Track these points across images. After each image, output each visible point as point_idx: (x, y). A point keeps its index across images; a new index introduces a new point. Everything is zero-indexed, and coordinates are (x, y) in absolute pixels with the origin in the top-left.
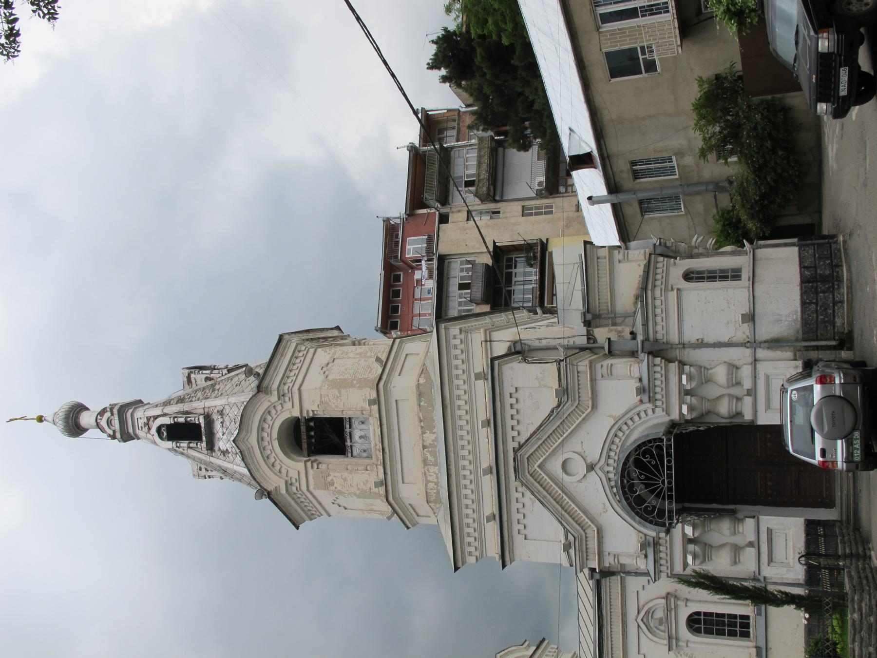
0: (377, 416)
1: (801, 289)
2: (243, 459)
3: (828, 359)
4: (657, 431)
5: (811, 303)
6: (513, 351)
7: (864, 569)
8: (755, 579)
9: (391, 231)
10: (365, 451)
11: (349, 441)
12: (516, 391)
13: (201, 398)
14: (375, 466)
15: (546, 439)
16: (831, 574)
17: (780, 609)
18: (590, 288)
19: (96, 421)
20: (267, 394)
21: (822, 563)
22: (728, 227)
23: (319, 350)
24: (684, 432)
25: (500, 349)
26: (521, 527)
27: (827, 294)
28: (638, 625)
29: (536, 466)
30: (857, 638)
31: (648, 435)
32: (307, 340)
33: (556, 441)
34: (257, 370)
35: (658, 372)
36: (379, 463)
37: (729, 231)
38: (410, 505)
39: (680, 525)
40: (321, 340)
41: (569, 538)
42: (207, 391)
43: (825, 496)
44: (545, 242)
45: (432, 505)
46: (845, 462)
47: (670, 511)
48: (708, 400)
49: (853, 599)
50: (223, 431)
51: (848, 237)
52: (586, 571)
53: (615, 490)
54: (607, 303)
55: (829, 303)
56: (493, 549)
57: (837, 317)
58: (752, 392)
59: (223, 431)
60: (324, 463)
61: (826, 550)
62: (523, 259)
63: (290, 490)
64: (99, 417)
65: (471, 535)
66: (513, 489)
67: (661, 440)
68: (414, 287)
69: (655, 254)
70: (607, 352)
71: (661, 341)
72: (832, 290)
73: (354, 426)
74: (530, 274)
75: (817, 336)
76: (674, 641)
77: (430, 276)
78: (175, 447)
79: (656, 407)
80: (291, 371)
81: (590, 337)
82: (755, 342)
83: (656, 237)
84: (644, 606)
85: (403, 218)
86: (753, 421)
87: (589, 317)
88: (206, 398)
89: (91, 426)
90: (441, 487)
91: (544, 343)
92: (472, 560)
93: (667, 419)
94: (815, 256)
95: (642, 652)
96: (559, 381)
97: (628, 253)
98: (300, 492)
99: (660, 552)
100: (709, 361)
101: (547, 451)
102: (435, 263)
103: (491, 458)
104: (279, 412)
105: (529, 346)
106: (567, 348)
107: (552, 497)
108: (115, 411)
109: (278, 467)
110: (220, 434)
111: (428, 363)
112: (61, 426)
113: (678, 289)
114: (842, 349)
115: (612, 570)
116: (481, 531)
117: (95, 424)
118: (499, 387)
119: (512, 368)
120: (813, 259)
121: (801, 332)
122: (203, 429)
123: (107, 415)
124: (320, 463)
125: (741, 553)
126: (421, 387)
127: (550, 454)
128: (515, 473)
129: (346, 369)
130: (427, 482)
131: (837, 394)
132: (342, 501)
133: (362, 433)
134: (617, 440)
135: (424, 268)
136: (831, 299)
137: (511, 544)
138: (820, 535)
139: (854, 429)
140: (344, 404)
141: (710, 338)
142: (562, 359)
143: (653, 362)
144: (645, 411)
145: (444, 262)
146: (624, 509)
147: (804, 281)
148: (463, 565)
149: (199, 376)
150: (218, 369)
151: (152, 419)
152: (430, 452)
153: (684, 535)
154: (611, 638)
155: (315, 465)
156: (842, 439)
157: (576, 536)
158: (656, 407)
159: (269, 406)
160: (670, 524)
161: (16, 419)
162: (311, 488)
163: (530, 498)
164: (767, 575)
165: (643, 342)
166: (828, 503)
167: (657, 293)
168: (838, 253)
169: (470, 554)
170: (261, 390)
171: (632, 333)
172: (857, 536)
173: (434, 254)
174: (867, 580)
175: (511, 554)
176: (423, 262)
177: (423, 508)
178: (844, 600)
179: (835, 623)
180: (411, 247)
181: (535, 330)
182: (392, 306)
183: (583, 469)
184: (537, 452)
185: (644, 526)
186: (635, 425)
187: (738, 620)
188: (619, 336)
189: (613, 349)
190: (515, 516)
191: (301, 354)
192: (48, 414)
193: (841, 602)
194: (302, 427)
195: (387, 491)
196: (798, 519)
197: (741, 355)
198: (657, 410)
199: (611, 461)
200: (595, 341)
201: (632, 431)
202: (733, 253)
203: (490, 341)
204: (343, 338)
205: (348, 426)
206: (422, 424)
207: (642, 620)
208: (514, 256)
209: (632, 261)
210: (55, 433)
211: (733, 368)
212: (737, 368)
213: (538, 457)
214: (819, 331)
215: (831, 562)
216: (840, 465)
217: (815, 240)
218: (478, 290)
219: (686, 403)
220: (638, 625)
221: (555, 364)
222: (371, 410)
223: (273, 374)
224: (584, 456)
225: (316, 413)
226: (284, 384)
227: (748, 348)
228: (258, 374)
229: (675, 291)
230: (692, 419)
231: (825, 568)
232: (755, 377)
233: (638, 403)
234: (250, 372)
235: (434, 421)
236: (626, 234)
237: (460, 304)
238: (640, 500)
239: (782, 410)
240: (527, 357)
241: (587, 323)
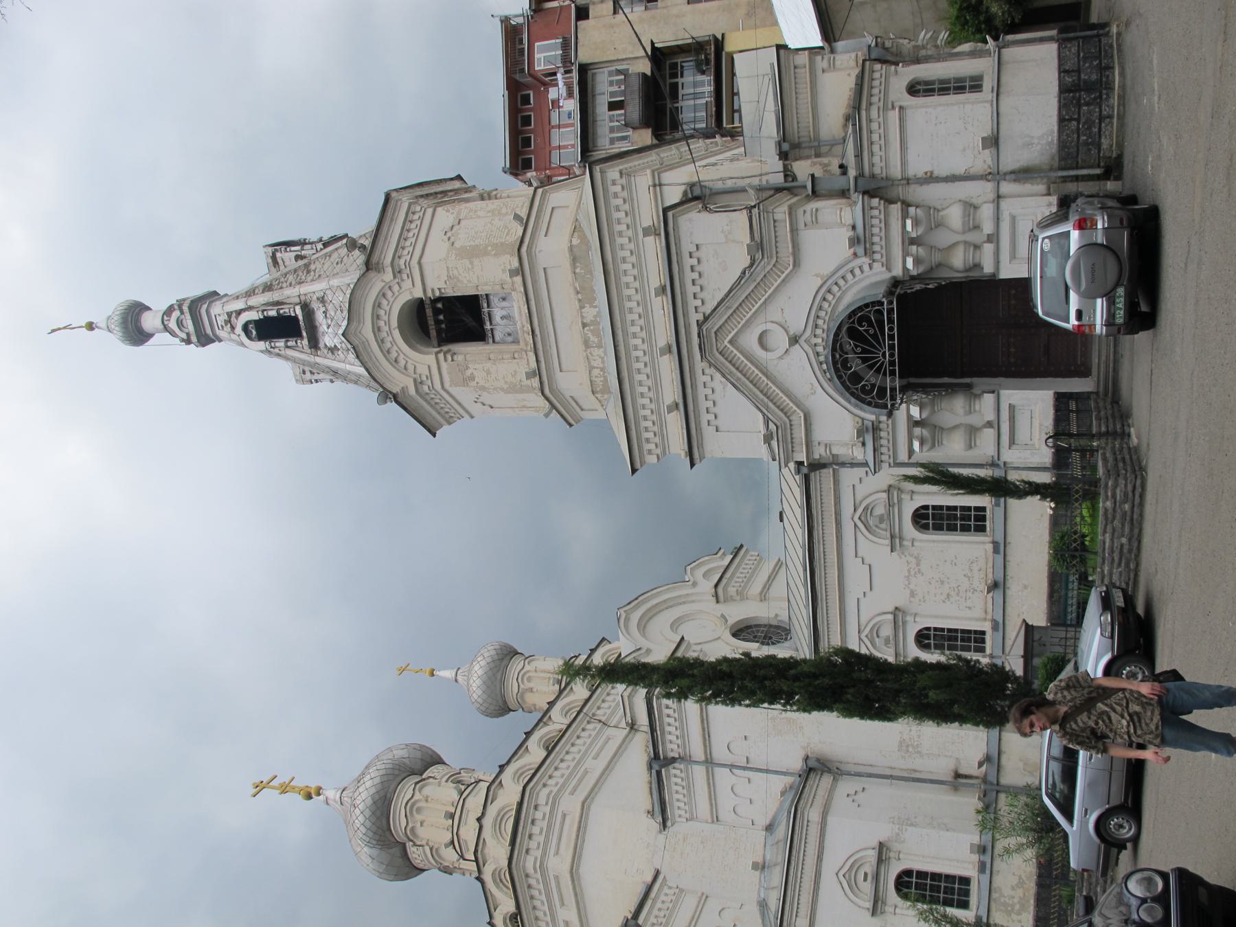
0: (522, 289)
1: (1059, 101)
2: (358, 357)
3: (1089, 193)
4: (875, 292)
5: (1071, 120)
6: (690, 196)
7: (1121, 450)
8: (993, 465)
9: (512, 34)
11: (488, 323)
12: (697, 249)
13: (294, 283)
14: (524, 353)
15: (737, 308)
16: (1083, 457)
17: (1022, 501)
18: (786, 108)
19: (163, 322)
20: (379, 272)
21: (1073, 445)
22: (965, 11)
23: (439, 210)
24: (909, 291)
25: (673, 195)
26: (711, 417)
27: (1092, 107)
28: (855, 524)
29: (726, 342)
30: (1109, 528)
31: (864, 298)
32: (422, 196)
33: (751, 310)
34: (362, 241)
35: (876, 217)
36: (529, 348)
37: (968, 17)
39: (904, 405)
40: (439, 196)
41: (770, 427)
42: (301, 274)
43: (1079, 363)
44: (720, 38)
45: (599, 396)
46: (1105, 325)
47: (893, 390)
48: (939, 249)
49: (1106, 485)
50: (327, 323)
51: (1124, 28)
52: (792, 465)
53: (824, 366)
54: (809, 127)
55: (1094, 119)
56: (678, 445)
57: (1103, 137)
58: (993, 238)
59: (327, 323)
60: (460, 354)
61: (1078, 427)
62: (691, 63)
63: (420, 391)
64: (165, 318)
65: (650, 429)
67: (881, 303)
68: (550, 110)
69: (870, 60)
70: (810, 192)
71: (879, 177)
72: (1098, 101)
73: (492, 304)
74: (702, 84)
75: (1077, 163)
76: (897, 540)
77: (570, 95)
78: (269, 348)
79: (874, 261)
80: (405, 240)
81: (788, 174)
82: (998, 173)
83: (872, 36)
84: (861, 502)
85: (528, 16)
86: (994, 275)
87: (786, 147)
88: (300, 283)
89: (157, 329)
90: (609, 373)
91: (729, 184)
92: (652, 459)
93: (887, 276)
94: (1079, 55)
95: (860, 554)
96: (751, 234)
97: (834, 58)
98: (434, 392)
99: (881, 438)
100: (940, 199)
101: (739, 323)
102: (575, 75)
103: (669, 334)
104: (397, 294)
105: (711, 189)
106: (760, 189)
107: (748, 379)
108: (185, 308)
109: (402, 363)
110: (325, 327)
111: (580, 217)
112: (117, 329)
113: (901, 108)
114: (1108, 179)
115: (823, 461)
116: (662, 424)
117: (162, 327)
118: (676, 244)
119: (690, 220)
120: (1076, 59)
121: (1057, 158)
122: (302, 323)
123: (176, 314)
124: (455, 354)
125: (978, 435)
126: (575, 250)
127: (742, 327)
128: (701, 351)
129: (476, 233)
130: (591, 368)
131: (1099, 241)
132: (486, 398)
133: (504, 313)
134: (826, 305)
135: (561, 84)
136: (1097, 114)
137: (700, 438)
138: (1072, 411)
139: (1117, 285)
140: (478, 277)
141: (941, 171)
142: (753, 204)
143: (869, 204)
144: (860, 267)
145: (587, 73)
146: (837, 390)
147: (1064, 89)
148: (641, 466)
149: (287, 254)
150: (310, 243)
151: (234, 314)
152: (591, 331)
153: (909, 417)
154: (824, 541)
155: (449, 357)
156: (1102, 298)
157: (779, 424)
158: (874, 261)
159: (383, 288)
160: (893, 405)
161: (59, 329)
162: (447, 385)
163: (721, 382)
164: (1008, 460)
165: (856, 178)
166: (1084, 372)
167: (874, 113)
168: (1110, 50)
169: (650, 452)
170: (370, 267)
171: (841, 166)
172: (1116, 410)
173: (572, 64)
174: (1124, 462)
175: (700, 448)
176: (559, 76)
177: (588, 400)
178: (1096, 487)
179: (1085, 512)
180: (542, 56)
181: (717, 167)
182: (522, 138)
184: (726, 325)
185: (861, 409)
186: (848, 285)
187: (973, 513)
188: (825, 171)
189: (817, 188)
190: (704, 405)
191: (416, 217)
192: (99, 320)
193: (1093, 489)
194: (427, 311)
195: (541, 383)
197: (981, 191)
198: (875, 265)
199: (819, 332)
200: (794, 179)
201: (844, 292)
202: (973, 54)
203: (660, 185)
204: (468, 190)
205: (485, 305)
206: (580, 296)
207: (859, 518)
208: (679, 61)
209: (839, 70)
210: (112, 343)
211: (970, 207)
212: (976, 208)
213: (728, 330)
214: (1080, 157)
215: (1083, 442)
216: (1099, 329)
217: (1080, 31)
218: (634, 109)
219: (912, 255)
220: (855, 524)
221: (745, 212)
222: (513, 283)
223: (383, 246)
224: (786, 327)
225: (443, 291)
226: (399, 257)
227: (989, 181)
228: (363, 247)
229: (897, 109)
230: (918, 275)
231: (1076, 450)
232: (998, 219)
233: (852, 257)
234: (353, 244)
235: (594, 291)
236: (829, 25)
237: (612, 130)
238: (856, 378)
239: (1030, 260)
240: (708, 204)
241: (783, 156)
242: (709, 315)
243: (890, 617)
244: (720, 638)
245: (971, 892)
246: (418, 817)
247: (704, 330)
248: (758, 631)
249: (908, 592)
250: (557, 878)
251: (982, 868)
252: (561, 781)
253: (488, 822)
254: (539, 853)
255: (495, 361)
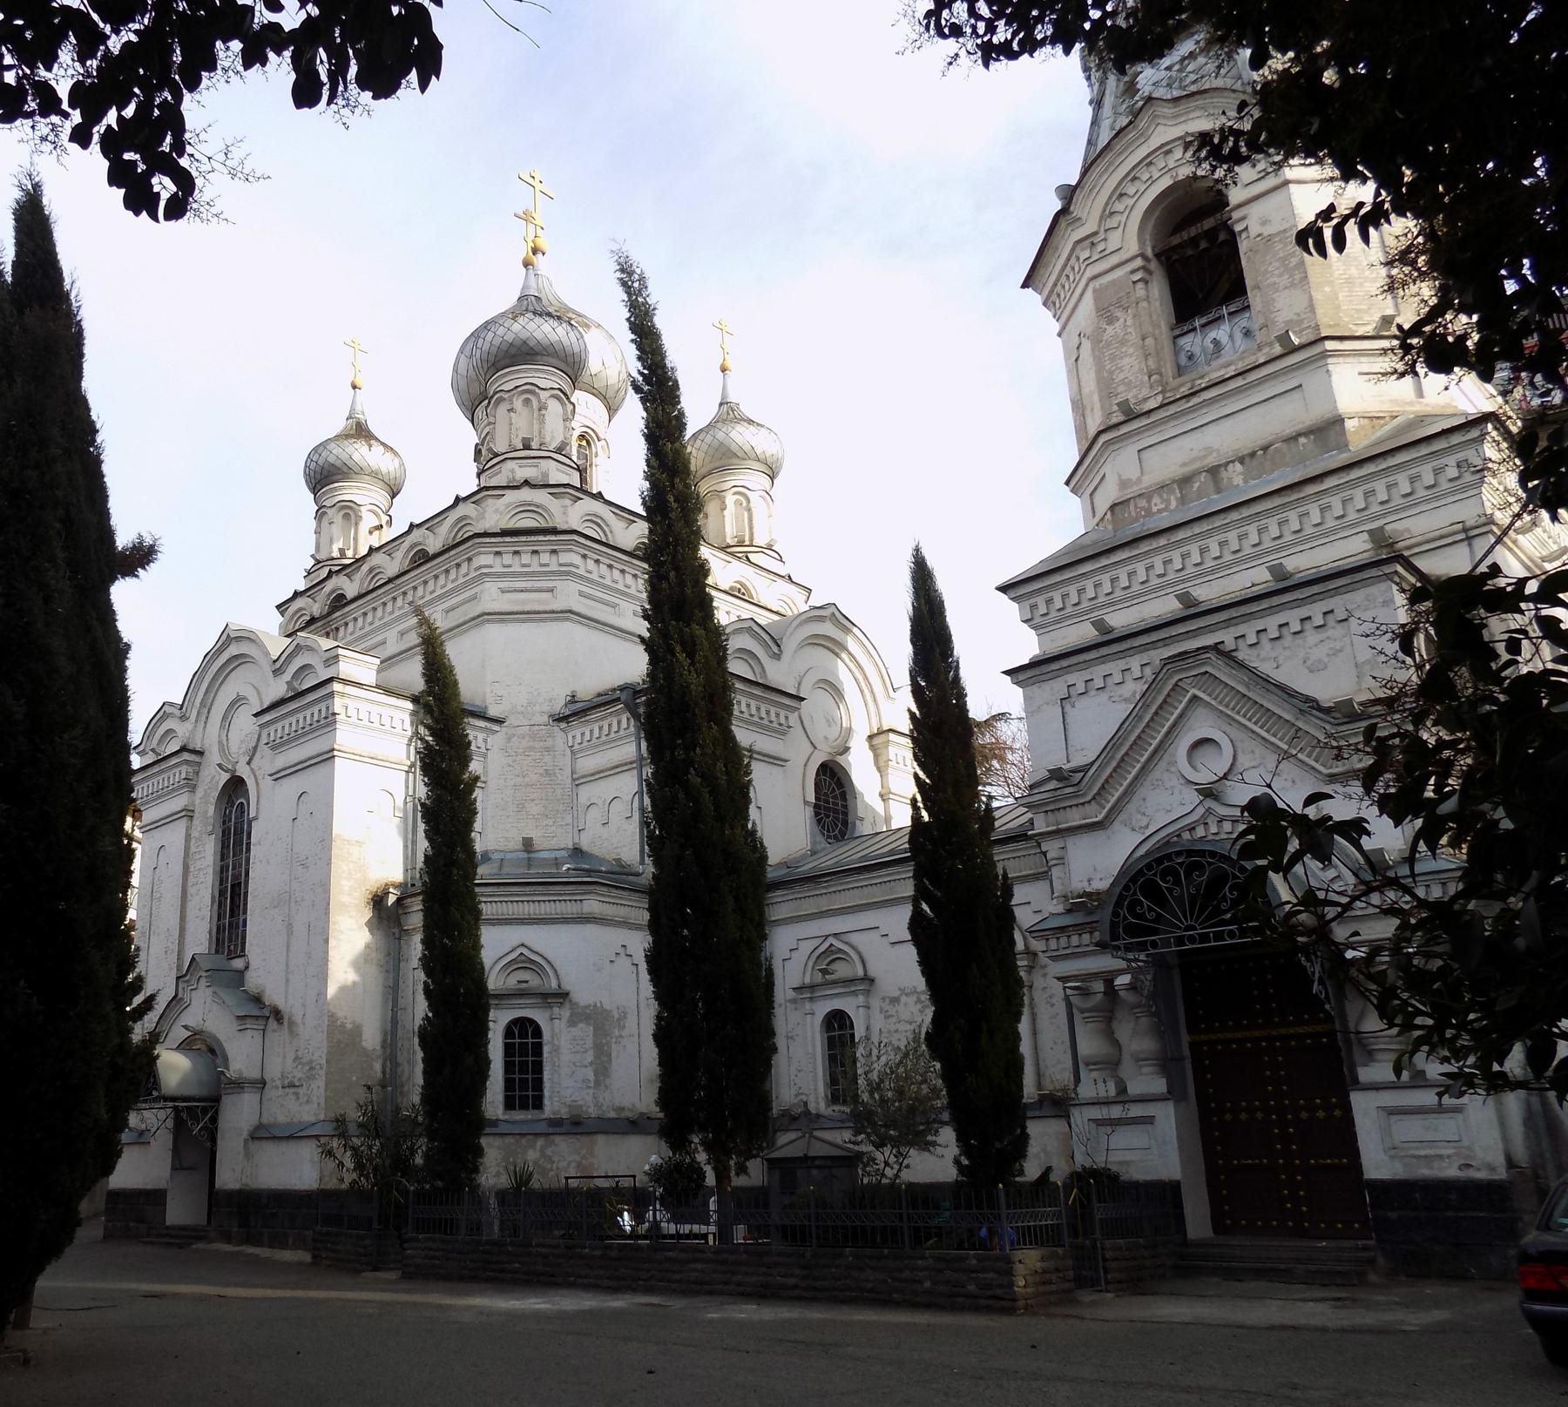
10: (1190, 358)
11: (1204, 320)
33: (1250, 720)
36: (1168, 395)
38: (1104, 475)
60: (1147, 289)
66: (1145, 657)
86: (1355, 1081)
107: (1143, 731)
128: (1174, 656)
137: (1049, 676)
160: (1117, 948)
183: (1204, 777)
196: (1179, 1170)
203: (1469, 539)
213: (1214, 691)
222: (1271, 344)
242: (1234, 659)
243: (860, 973)
244: (815, 748)
245: (525, 1112)
246: (518, 403)
247: (1208, 655)
248: (835, 797)
249: (896, 994)
250: (474, 598)
251: (556, 1123)
252: (595, 576)
253: (526, 494)
254: (498, 569)
255: (1144, 346)
